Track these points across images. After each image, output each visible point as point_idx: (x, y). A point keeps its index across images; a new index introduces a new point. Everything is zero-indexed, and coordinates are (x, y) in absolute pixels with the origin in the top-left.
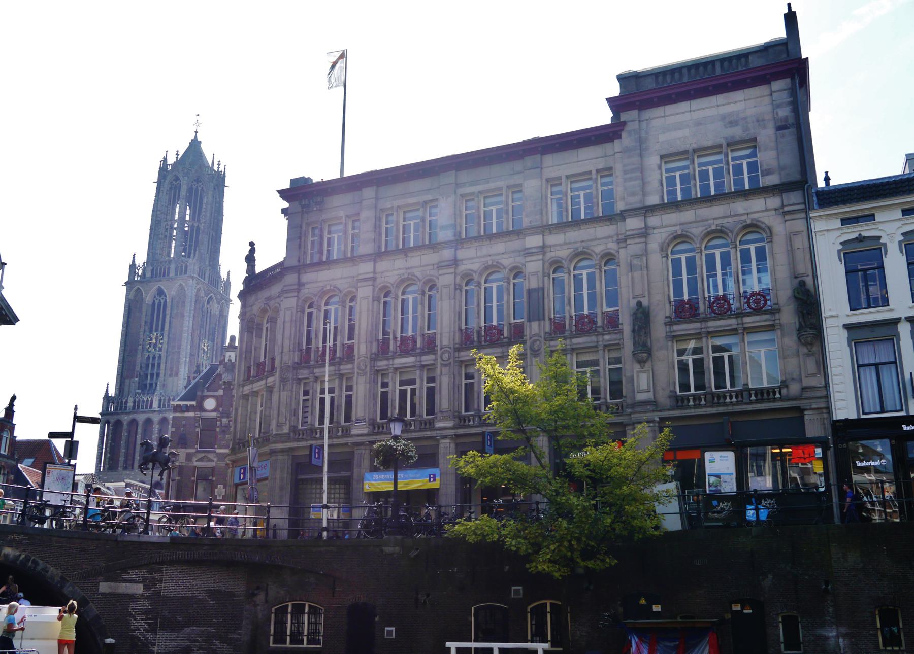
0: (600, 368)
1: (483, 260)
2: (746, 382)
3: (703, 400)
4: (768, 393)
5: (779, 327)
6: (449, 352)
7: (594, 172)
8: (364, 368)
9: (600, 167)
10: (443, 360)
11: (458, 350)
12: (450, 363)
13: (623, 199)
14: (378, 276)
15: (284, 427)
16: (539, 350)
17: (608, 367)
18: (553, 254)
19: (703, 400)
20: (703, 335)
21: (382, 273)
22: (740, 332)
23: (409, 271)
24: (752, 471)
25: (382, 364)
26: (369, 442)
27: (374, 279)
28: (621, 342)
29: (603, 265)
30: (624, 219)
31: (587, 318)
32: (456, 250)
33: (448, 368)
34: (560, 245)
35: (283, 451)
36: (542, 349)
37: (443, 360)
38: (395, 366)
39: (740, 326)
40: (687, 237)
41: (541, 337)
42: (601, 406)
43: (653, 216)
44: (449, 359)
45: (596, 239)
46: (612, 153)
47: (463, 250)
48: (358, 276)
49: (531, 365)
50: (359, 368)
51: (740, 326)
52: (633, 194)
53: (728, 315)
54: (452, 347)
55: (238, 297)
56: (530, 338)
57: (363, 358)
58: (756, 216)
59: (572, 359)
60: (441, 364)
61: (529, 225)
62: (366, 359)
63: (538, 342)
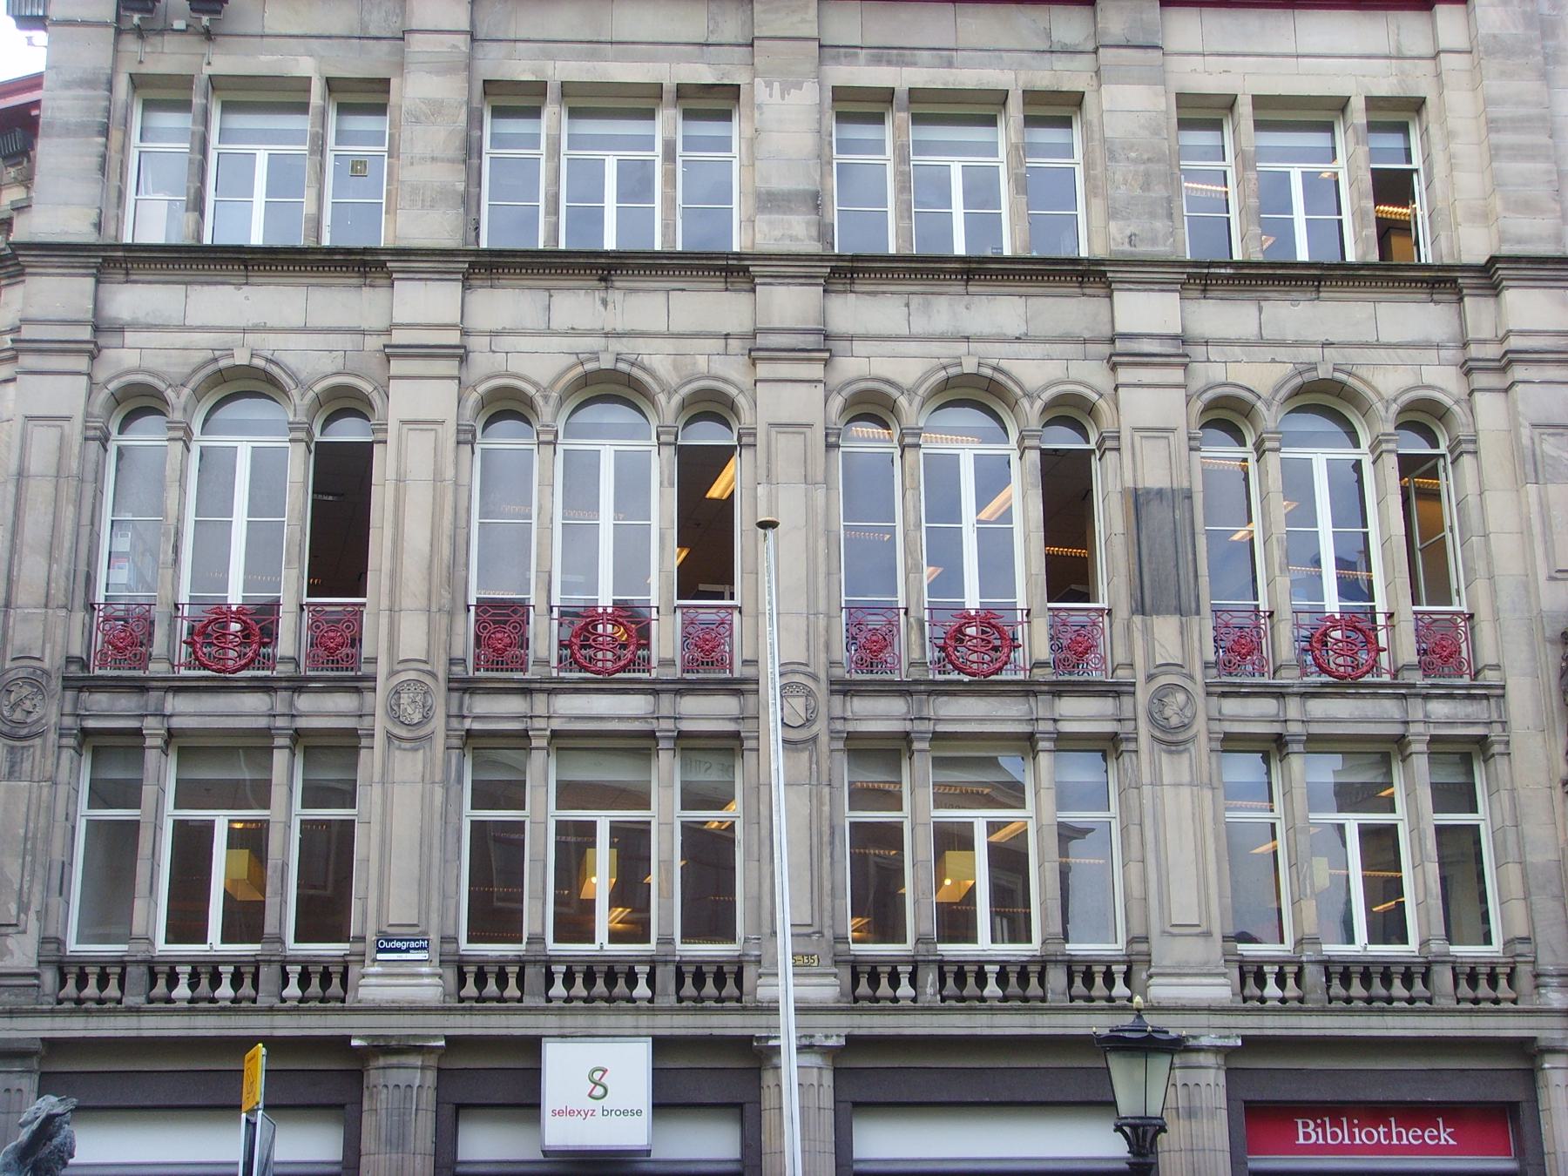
1: (935, 348)
2: (539, 930)
3: (642, 982)
6: (809, 694)
7: (200, 83)
9: (1384, 89)
11: (463, 687)
12: (815, 739)
13: (1484, 216)
14: (477, 343)
15: (11, 942)
16: (1184, 726)
18: (1216, 373)
19: (642, 982)
20: (278, 741)
21: (494, 334)
23: (617, 346)
27: (461, 355)
28: (1495, 732)
29: (114, 430)
30: (1495, 289)
31: (239, 620)
33: (805, 756)
34: (1246, 343)
36: (1200, 726)
38: (556, 725)
40: (272, 380)
41: (1191, 677)
42: (1435, 968)
43: (247, 284)
44: (809, 722)
45: (1378, 345)
46: (1425, 48)
48: (388, 332)
49: (1157, 782)
50: (394, 714)
51: (666, 725)
52: (1527, 207)
53: (48, 682)
54: (822, 676)
56: (1150, 678)
57: (412, 675)
58: (269, 343)
59: (75, 772)
61: (1127, 247)
62: (428, 680)
63: (1181, 697)
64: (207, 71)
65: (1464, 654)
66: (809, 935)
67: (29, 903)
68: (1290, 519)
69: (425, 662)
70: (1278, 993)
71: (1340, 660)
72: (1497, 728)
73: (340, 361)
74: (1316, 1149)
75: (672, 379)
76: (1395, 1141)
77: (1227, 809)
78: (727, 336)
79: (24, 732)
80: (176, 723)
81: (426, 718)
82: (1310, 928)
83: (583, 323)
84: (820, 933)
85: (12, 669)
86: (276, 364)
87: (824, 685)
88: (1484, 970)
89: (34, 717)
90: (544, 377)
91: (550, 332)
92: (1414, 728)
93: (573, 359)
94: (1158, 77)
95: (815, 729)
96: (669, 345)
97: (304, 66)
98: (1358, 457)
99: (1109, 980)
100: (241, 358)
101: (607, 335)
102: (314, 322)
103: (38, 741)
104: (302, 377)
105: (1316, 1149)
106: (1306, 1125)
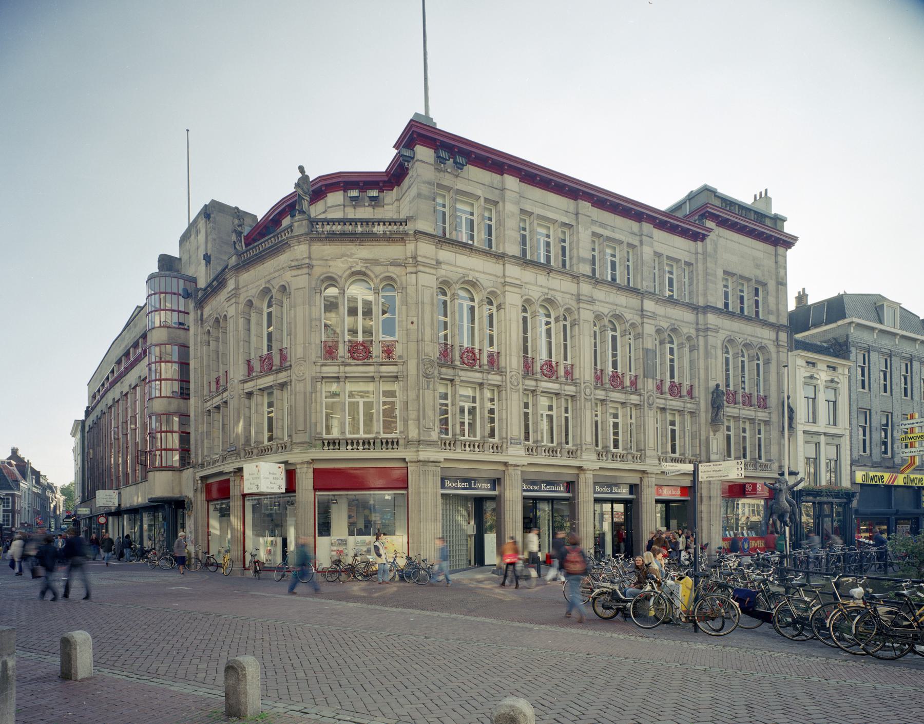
2: (378, 431)
4: (552, 451)
5: (402, 379)
6: (590, 388)
8: (516, 384)
21: (526, 283)
22: (376, 379)
23: (551, 292)
24: (878, 549)
30: (705, 313)
32: (310, 246)
38: (541, 389)
39: (377, 374)
44: (590, 395)
51: (377, 374)
55: (160, 256)
56: (295, 363)
58: (477, 275)
60: (585, 398)
64: (456, 187)
72: (578, 394)
77: (460, 401)
78: (572, 294)
80: (462, 378)
89: (431, 373)
90: (455, 279)
91: (536, 284)
92: (539, 388)
94: (652, 246)
96: (561, 294)
97: (479, 192)
100: (471, 278)
103: (433, 380)
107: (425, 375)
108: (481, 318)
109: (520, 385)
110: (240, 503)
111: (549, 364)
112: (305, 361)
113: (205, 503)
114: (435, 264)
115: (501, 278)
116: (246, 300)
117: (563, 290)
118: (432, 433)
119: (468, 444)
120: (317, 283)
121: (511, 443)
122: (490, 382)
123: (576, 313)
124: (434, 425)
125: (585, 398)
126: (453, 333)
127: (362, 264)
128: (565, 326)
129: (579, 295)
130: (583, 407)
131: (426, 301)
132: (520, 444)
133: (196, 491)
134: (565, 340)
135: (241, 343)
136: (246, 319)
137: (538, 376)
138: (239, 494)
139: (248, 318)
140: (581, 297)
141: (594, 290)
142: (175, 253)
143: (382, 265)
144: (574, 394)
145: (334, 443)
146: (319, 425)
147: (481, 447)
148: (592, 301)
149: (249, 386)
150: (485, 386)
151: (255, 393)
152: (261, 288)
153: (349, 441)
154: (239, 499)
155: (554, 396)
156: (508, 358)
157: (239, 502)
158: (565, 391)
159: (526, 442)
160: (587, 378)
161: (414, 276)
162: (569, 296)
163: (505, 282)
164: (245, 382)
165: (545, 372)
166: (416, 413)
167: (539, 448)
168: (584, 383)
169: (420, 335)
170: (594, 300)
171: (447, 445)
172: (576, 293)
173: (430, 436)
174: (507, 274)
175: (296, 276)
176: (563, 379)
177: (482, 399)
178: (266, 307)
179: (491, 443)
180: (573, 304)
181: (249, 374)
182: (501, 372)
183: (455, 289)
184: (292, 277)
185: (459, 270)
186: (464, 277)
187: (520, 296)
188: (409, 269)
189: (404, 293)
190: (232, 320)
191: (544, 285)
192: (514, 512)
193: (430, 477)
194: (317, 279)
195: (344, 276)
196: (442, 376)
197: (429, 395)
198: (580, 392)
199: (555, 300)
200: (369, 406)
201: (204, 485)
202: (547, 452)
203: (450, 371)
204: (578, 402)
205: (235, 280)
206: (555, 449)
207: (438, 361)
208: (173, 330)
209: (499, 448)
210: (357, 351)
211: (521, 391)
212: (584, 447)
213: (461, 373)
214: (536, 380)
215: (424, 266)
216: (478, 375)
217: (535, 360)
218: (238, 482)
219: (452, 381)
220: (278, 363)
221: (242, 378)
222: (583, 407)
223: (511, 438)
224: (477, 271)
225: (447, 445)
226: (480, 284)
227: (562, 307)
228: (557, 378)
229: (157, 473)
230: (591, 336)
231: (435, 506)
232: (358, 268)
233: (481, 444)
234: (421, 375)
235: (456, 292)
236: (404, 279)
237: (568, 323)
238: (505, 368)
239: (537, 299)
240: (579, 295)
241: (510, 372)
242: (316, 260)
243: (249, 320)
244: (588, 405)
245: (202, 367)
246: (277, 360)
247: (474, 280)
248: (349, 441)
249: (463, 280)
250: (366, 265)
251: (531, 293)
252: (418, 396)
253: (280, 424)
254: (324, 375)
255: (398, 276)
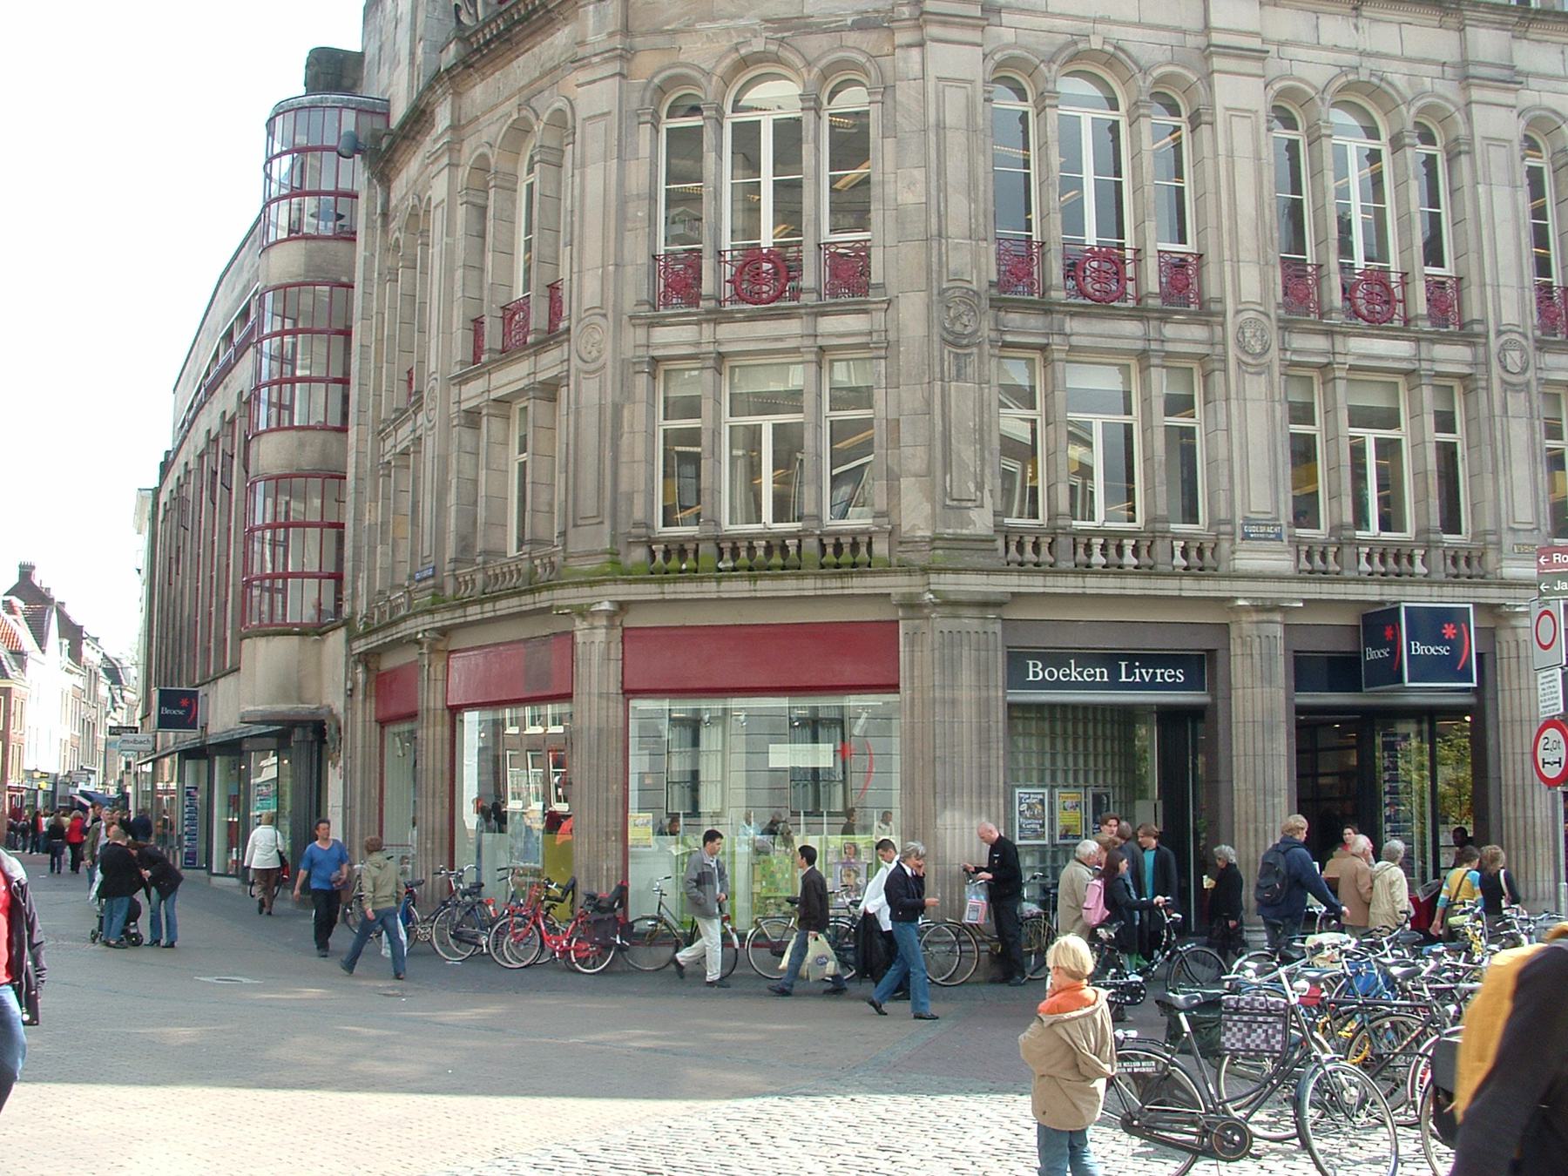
0: (1402, 433)
6: (1523, 350)
8: (1258, 349)
10: (1504, 368)
17: (662, 425)
21: (1281, 44)
25: (1451, 357)
26: (1304, 601)
31: (769, 261)
33: (1522, 395)
35: (985, 604)
37: (1504, 368)
38: (1350, 360)
44: (1524, 370)
47: (1525, 41)
50: (1242, 347)
56: (578, 323)
57: (1252, 314)
58: (1117, 33)
60: (1504, 382)
62: (1262, 318)
65: (1036, 276)
66: (1532, 530)
67: (983, 482)
68: (1063, 168)
69: (1260, 304)
70: (1135, 562)
71: (1097, 286)
73: (1169, 54)
74: (1043, 685)
75: (1409, 95)
76: (1098, 679)
78: (1444, 64)
79: (965, 342)
80: (1075, 340)
81: (1265, 351)
82: (1162, 510)
83: (1344, 42)
84: (1538, 529)
85: (949, 289)
86: (1123, 51)
87: (1531, 342)
88: (1463, 554)
89: (969, 330)
91: (1318, 46)
93: (1337, 70)
95: (1528, 375)
96: (1404, 67)
98: (1025, 109)
99: (1036, 547)
100: (1096, 43)
101: (1361, 54)
102: (1149, 18)
103: (975, 350)
104: (1142, 63)
105: (1043, 685)
106: (1035, 666)
107: (950, 338)
108: (1136, 155)
109: (1274, 353)
110: (442, 731)
111: (1379, 279)
112: (605, 316)
113: (376, 728)
114: (979, 14)
115: (1197, 33)
116: (477, 153)
117: (1407, 53)
118: (973, 514)
119: (1097, 542)
120: (643, 101)
121: (1246, 537)
122: (1169, 347)
123: (1459, 117)
124: (980, 487)
125: (1504, 382)
126: (1045, 209)
127: (769, 34)
128: (1430, 162)
129: (1465, 63)
130: (1498, 410)
131: (950, 120)
132: (1279, 537)
133: (350, 693)
134: (1434, 201)
135: (459, 273)
136: (474, 205)
137: (1337, 319)
138: (440, 705)
139: (479, 201)
140: (1472, 70)
141: (1517, 45)
142: (351, 41)
143: (825, 31)
144: (1467, 370)
145: (682, 553)
146: (639, 501)
147: (1144, 552)
148: (1512, 78)
149: (473, 394)
150: (1154, 361)
151: (484, 412)
152: (510, 121)
153: (727, 545)
154: (439, 718)
155: (1401, 380)
156: (1227, 269)
157: (439, 728)
158: (1432, 361)
159: (1300, 532)
160: (1510, 315)
161: (915, 53)
162: (1435, 70)
163: (1209, 46)
164: (463, 379)
165: (1361, 304)
166: (921, 452)
167: (1347, 550)
168: (1499, 333)
169: (934, 220)
170: (1519, 73)
171: (1029, 548)
172: (1456, 58)
173: (970, 522)
174: (1215, 21)
175: (589, 83)
176: (1426, 326)
177: (1146, 400)
178: (525, 173)
179: (1176, 537)
180: (1448, 90)
181: (476, 359)
182: (1207, 313)
183: (1047, 81)
184: (578, 86)
185: (1060, 23)
186: (1076, 43)
187: (1261, 83)
188: (902, 38)
189: (889, 102)
190: (439, 210)
191: (1344, 43)
192: (1259, 762)
193: (967, 655)
194: (645, 87)
195: (719, 71)
196: (1009, 338)
197: (963, 397)
198: (1487, 363)
199: (1383, 85)
200: (787, 441)
201: (373, 678)
202: (1376, 559)
203: (1035, 321)
204: (1483, 395)
205: (453, 105)
206: (1405, 551)
207: (994, 291)
208: (322, 244)
209: (1208, 554)
210: (757, 275)
211: (1276, 370)
212: (1508, 540)
213: (1071, 325)
214: (1330, 333)
215: (944, 24)
216: (1132, 327)
217: (1324, 271)
218: (439, 668)
219: (1043, 348)
220: (544, 325)
221: (457, 370)
222: (1498, 410)
223: (1248, 521)
224: (1116, 22)
225: (1029, 548)
226: (1129, 56)
227: (1409, 103)
228: (1407, 322)
229: (261, 643)
230: (1514, 187)
231: (984, 744)
232: (758, 45)
233: (1145, 544)
234: (936, 338)
235: (1050, 87)
236: (886, 62)
237: (1438, 151)
238: (1221, 301)
239: (1321, 88)
240: (1465, 63)
241: (1238, 312)
242: (643, 35)
243: (483, 210)
244: (1517, 402)
245: (380, 341)
246: (538, 317)
247: (1110, 49)
248: (727, 545)
249: (1072, 50)
250: (779, 35)
251: (1299, 70)
252: (929, 403)
253: (544, 497)
254: (657, 353)
255: (871, 57)
